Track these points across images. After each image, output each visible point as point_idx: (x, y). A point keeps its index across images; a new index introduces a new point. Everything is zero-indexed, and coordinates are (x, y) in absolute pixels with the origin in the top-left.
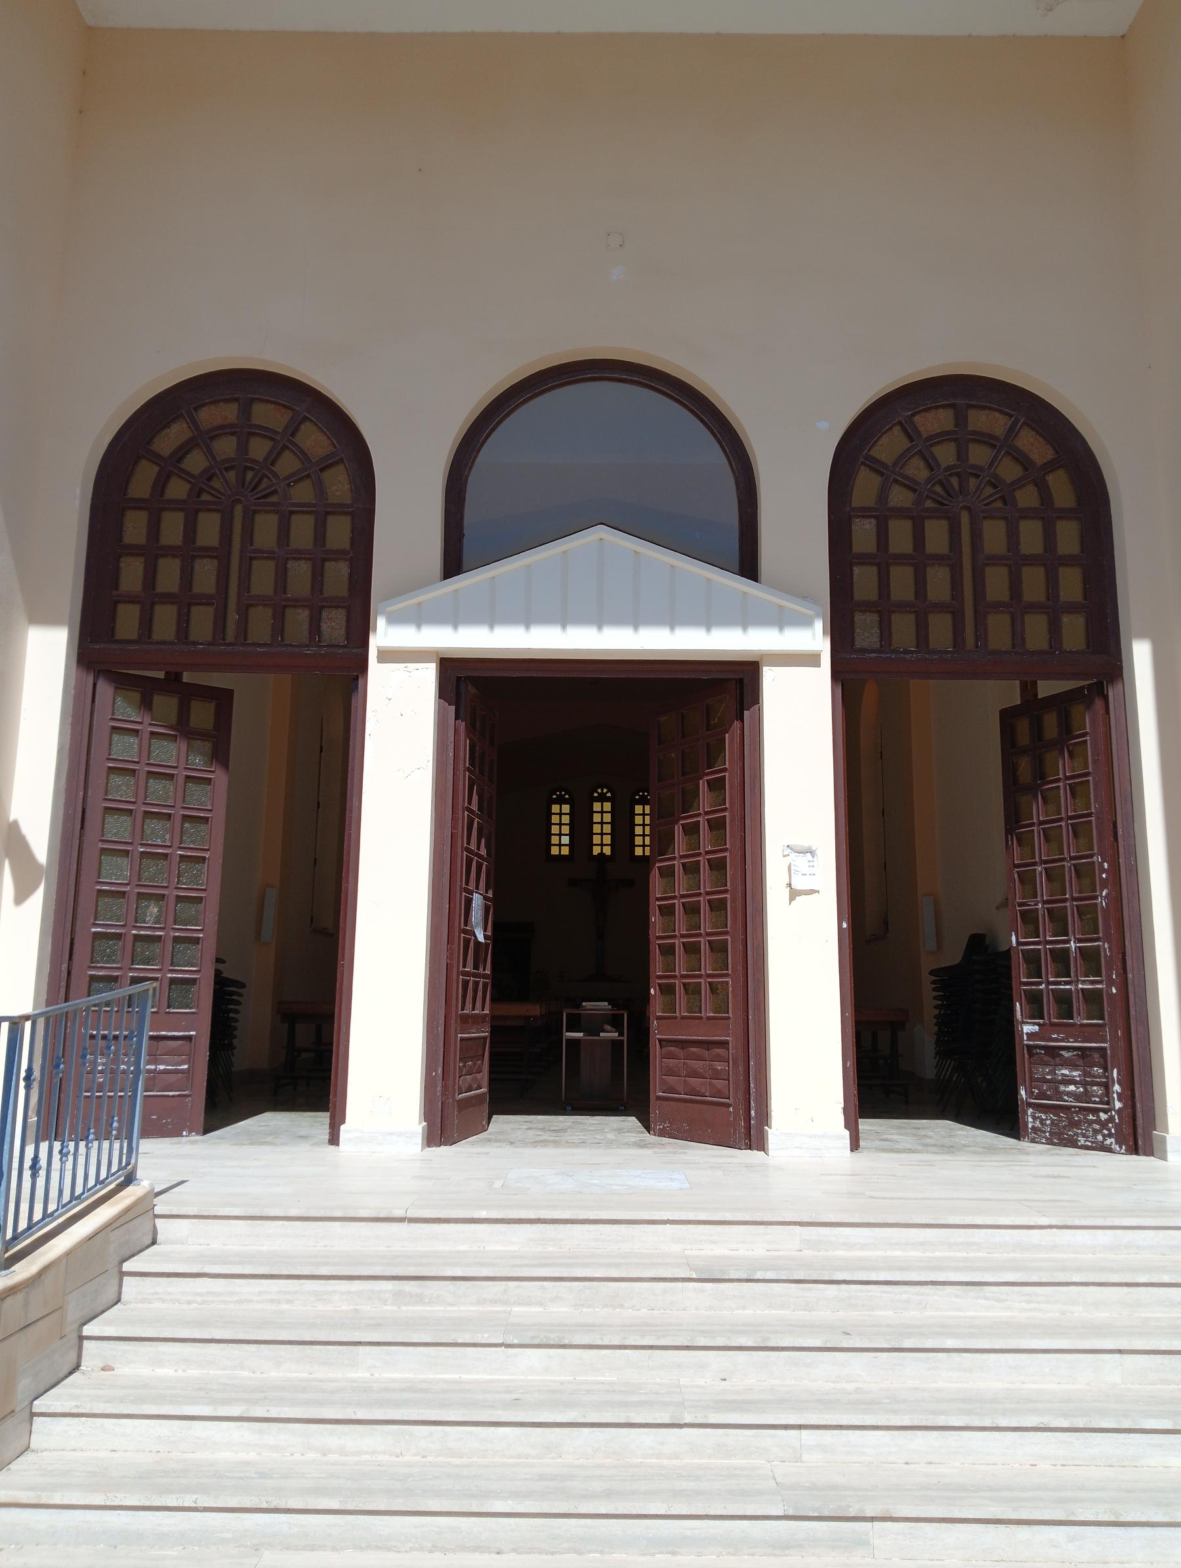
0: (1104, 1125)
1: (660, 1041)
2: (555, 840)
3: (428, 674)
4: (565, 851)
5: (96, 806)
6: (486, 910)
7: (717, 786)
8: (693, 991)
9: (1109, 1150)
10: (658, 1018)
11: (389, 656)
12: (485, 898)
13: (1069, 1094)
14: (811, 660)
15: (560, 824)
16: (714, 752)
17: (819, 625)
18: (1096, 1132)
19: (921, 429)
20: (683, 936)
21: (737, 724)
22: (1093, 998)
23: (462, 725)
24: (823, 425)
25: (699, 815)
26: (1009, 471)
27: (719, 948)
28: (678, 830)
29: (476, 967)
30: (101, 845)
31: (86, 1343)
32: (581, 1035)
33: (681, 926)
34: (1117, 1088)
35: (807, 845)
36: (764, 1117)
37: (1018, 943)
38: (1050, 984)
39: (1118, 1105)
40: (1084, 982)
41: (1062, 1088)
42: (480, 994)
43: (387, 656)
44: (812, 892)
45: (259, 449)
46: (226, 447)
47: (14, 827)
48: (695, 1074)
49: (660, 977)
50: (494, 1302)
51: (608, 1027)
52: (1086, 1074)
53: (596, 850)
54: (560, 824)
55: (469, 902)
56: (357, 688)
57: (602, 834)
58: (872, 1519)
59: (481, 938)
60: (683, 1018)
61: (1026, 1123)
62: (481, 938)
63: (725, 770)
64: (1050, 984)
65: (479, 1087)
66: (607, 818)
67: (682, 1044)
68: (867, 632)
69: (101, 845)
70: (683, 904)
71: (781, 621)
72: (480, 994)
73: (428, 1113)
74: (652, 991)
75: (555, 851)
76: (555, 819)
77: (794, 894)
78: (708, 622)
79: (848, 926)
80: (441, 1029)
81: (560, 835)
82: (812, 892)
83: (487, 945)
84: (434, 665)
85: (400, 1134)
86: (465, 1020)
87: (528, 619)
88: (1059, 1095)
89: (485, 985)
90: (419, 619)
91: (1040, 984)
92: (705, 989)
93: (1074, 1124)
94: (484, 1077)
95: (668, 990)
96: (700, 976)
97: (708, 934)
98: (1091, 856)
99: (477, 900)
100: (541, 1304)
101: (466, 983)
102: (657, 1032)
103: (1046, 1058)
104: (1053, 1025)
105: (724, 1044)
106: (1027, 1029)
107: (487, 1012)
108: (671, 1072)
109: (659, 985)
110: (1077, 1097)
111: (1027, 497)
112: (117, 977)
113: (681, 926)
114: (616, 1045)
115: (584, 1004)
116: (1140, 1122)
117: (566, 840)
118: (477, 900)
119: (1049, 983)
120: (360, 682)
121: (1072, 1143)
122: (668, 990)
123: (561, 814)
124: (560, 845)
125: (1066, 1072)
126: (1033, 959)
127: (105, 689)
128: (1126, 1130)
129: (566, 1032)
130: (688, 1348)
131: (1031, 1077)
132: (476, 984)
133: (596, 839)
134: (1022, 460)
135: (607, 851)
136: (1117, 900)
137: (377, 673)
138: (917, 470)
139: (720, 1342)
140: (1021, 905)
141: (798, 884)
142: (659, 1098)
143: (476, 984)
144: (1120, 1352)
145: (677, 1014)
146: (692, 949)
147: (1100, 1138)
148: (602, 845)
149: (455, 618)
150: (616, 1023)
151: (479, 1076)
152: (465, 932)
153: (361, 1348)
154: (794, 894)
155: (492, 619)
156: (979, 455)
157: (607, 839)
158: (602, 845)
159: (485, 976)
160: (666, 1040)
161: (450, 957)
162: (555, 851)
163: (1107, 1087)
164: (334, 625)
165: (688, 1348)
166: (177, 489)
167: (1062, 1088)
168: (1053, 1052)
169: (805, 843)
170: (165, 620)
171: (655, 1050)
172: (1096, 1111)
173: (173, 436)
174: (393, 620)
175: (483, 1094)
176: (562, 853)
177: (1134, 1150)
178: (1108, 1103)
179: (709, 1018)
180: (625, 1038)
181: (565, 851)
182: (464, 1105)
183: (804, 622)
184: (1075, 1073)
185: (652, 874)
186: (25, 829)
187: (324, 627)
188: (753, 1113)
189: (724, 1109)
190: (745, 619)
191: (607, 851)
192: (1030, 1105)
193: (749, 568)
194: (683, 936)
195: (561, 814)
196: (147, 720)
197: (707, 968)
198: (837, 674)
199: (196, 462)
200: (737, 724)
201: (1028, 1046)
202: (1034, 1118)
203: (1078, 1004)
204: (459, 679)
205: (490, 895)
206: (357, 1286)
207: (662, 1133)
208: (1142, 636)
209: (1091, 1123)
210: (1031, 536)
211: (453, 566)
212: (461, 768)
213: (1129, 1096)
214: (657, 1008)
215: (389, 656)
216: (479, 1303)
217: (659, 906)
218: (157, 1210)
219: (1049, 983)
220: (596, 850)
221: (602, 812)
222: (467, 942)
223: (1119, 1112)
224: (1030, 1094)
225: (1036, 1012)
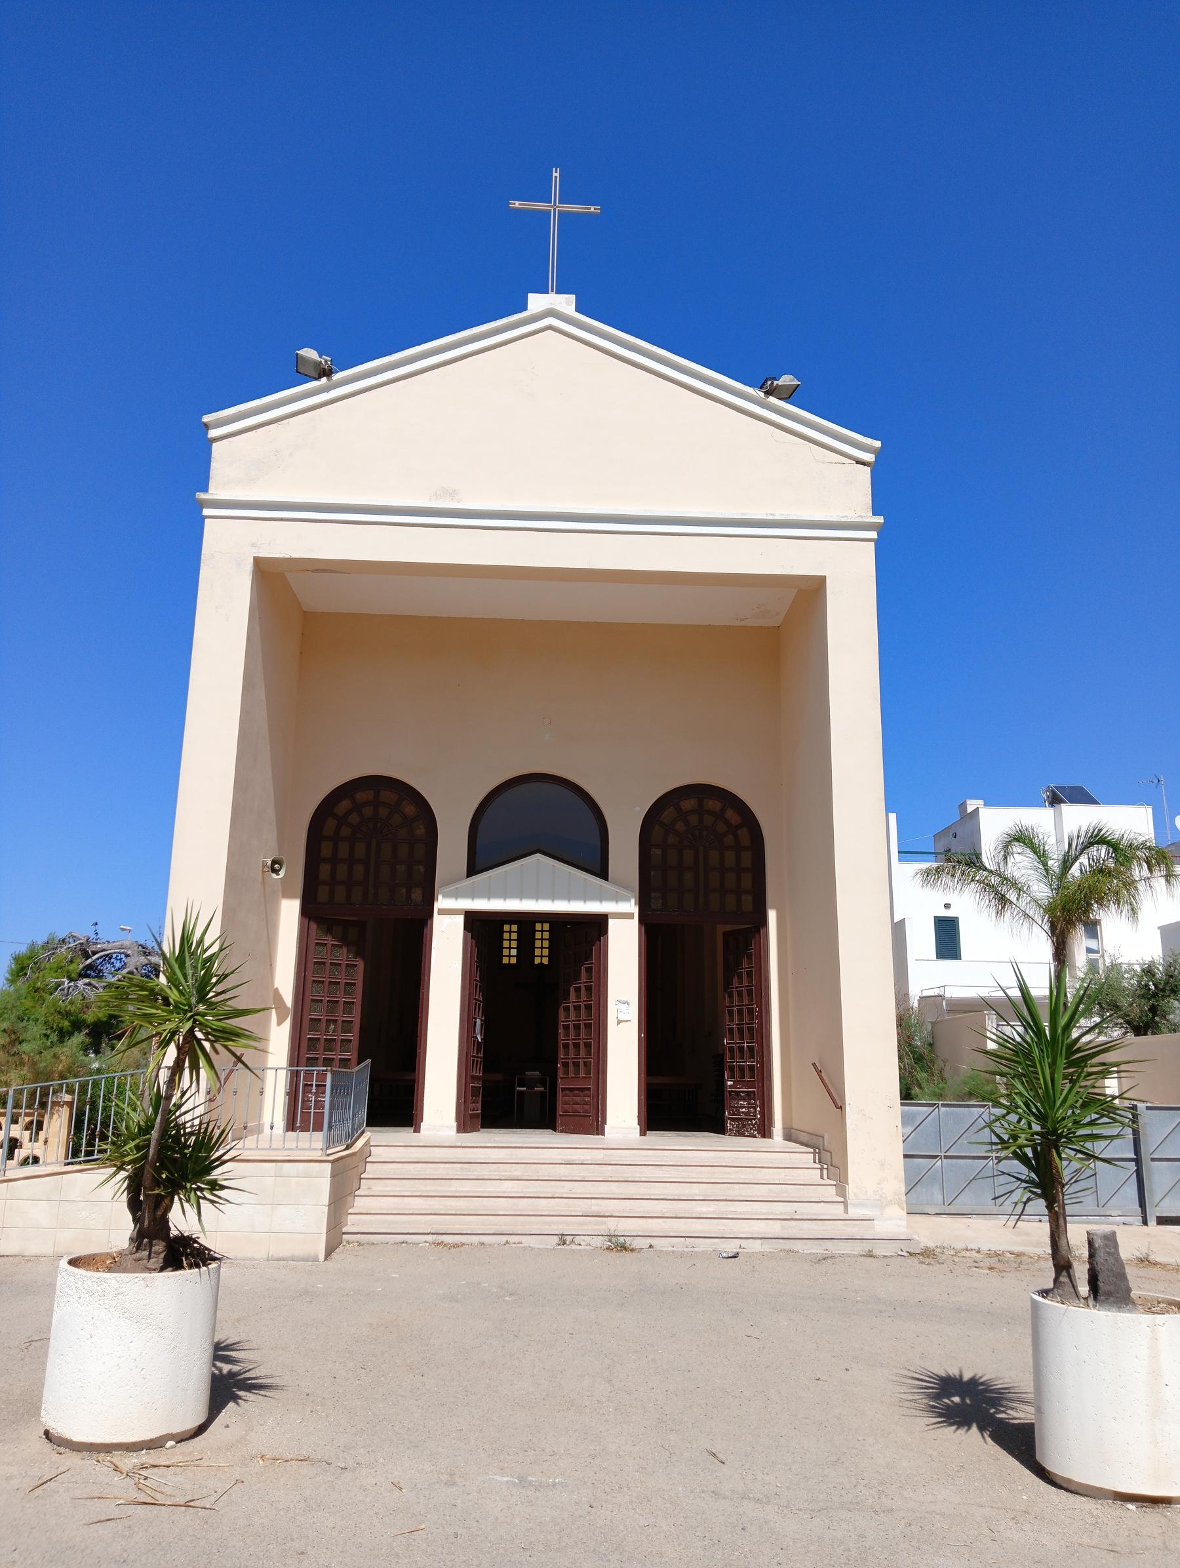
0: (754, 1125)
1: (562, 1088)
2: (505, 952)
3: (460, 919)
4: (513, 961)
5: (310, 979)
6: (482, 1025)
7: (589, 970)
8: (576, 1065)
9: (754, 1136)
10: (561, 1078)
11: (443, 912)
12: (482, 1020)
13: (743, 1112)
14: (629, 916)
15: (510, 940)
16: (588, 956)
17: (633, 901)
18: (751, 1129)
19: (683, 808)
20: (573, 1039)
21: (598, 942)
22: (751, 1068)
23: (474, 942)
24: (638, 809)
25: (570, 1003)
26: (721, 828)
27: (588, 1045)
28: (572, 989)
29: (477, 1054)
30: (311, 997)
31: (362, 1180)
32: (525, 1089)
33: (572, 1035)
34: (758, 1109)
35: (625, 1000)
36: (604, 1121)
37: (727, 1043)
38: (737, 1062)
39: (759, 1116)
40: (749, 1062)
41: (741, 1110)
42: (479, 1065)
43: (442, 912)
44: (627, 1021)
45: (383, 812)
46: (368, 811)
47: (276, 991)
48: (577, 1103)
49: (562, 1059)
50: (495, 1171)
51: (539, 1085)
52: (749, 1103)
53: (537, 961)
54: (510, 940)
55: (475, 1022)
56: (427, 925)
57: (542, 948)
58: (608, 1216)
59: (480, 1040)
60: (572, 1077)
61: (727, 1127)
62: (480, 1040)
63: (592, 963)
64: (737, 1062)
65: (477, 1110)
66: (546, 935)
67: (571, 1090)
68: (657, 904)
69: (311, 997)
70: (574, 1024)
71: (617, 898)
72: (479, 1065)
73: (458, 1119)
74: (559, 1065)
75: (505, 960)
76: (506, 936)
77: (619, 1022)
78: (585, 898)
79: (644, 1036)
80: (463, 1081)
81: (510, 948)
82: (627, 1021)
83: (481, 1043)
84: (463, 916)
85: (447, 1127)
86: (474, 1078)
87: (505, 896)
88: (739, 1113)
89: (481, 1062)
90: (457, 895)
91: (734, 1062)
92: (582, 1064)
93: (744, 1126)
94: (479, 1105)
95: (566, 1065)
96: (569, 1058)
97: (584, 1039)
98: (752, 1005)
99: (478, 1022)
100: (510, 1172)
101: (473, 1060)
102: (561, 1084)
103: (735, 1097)
104: (738, 1081)
105: (589, 1089)
106: (729, 1083)
107: (481, 1074)
108: (566, 1103)
109: (562, 1062)
110: (745, 1114)
111: (729, 840)
112: (318, 1058)
113: (572, 1035)
114: (542, 1094)
115: (527, 1073)
116: (766, 1123)
117: (514, 952)
118: (478, 1022)
119: (737, 1062)
120: (429, 922)
121: (743, 1135)
122: (566, 1065)
123: (510, 932)
124: (510, 956)
125: (742, 1102)
126: (731, 1050)
127: (313, 926)
128: (761, 1128)
129: (518, 1087)
130: (559, 1180)
131: (730, 1106)
132: (477, 1061)
133: (537, 952)
134: (727, 822)
135: (546, 961)
136: (761, 1025)
137: (437, 919)
138: (680, 826)
139: (570, 1179)
140: (728, 1025)
141: (622, 1017)
142: (561, 1115)
143: (477, 1061)
144: (699, 1183)
145: (570, 1076)
146: (577, 1046)
147: (752, 1131)
148: (542, 956)
149: (473, 895)
150: (543, 1084)
151: (478, 1105)
152: (473, 1037)
153: (453, 1181)
154: (619, 1022)
155: (489, 896)
156: (708, 820)
157: (546, 952)
158: (542, 956)
159: (480, 1058)
160: (564, 1088)
161: (467, 1049)
162: (505, 960)
163: (755, 1108)
164: (417, 895)
165: (559, 1180)
166: (345, 831)
167: (741, 1110)
168: (738, 1093)
169: (625, 999)
170: (341, 892)
171: (559, 1092)
172: (752, 1119)
173: (345, 805)
174: (444, 896)
175: (479, 1113)
176: (509, 926)
177: (764, 1136)
178: (755, 1116)
179: (583, 1077)
180: (548, 1091)
181: (513, 961)
182: (472, 1116)
183: (628, 900)
184: (745, 1103)
185: (560, 1010)
186: (282, 992)
187: (413, 896)
188: (600, 1119)
189: (588, 1118)
190: (601, 898)
191: (546, 961)
192: (729, 1118)
193: (603, 874)
194: (573, 1039)
195: (510, 932)
196: (330, 938)
197: (582, 1054)
198: (641, 921)
199: (354, 818)
200: (598, 942)
201: (729, 1091)
202: (730, 1124)
203: (747, 1071)
204: (473, 920)
205: (483, 1019)
206: (447, 1166)
207: (562, 1131)
208: (772, 908)
209: (750, 1125)
210: (730, 857)
211: (472, 871)
212: (473, 962)
213: (762, 1113)
214: (561, 1074)
215: (443, 912)
216: (489, 1172)
217: (563, 1025)
218: (371, 1144)
219: (737, 1062)
220: (537, 961)
221: (542, 931)
222: (474, 1041)
223: (759, 1119)
224: (729, 1114)
225: (732, 1076)
